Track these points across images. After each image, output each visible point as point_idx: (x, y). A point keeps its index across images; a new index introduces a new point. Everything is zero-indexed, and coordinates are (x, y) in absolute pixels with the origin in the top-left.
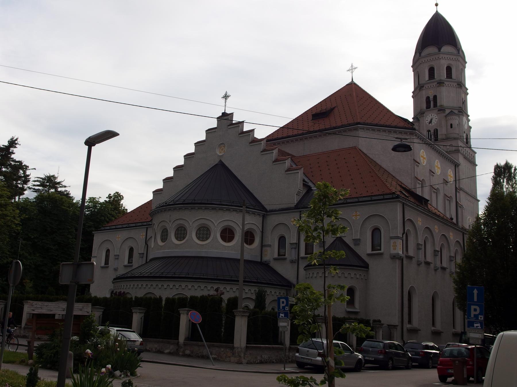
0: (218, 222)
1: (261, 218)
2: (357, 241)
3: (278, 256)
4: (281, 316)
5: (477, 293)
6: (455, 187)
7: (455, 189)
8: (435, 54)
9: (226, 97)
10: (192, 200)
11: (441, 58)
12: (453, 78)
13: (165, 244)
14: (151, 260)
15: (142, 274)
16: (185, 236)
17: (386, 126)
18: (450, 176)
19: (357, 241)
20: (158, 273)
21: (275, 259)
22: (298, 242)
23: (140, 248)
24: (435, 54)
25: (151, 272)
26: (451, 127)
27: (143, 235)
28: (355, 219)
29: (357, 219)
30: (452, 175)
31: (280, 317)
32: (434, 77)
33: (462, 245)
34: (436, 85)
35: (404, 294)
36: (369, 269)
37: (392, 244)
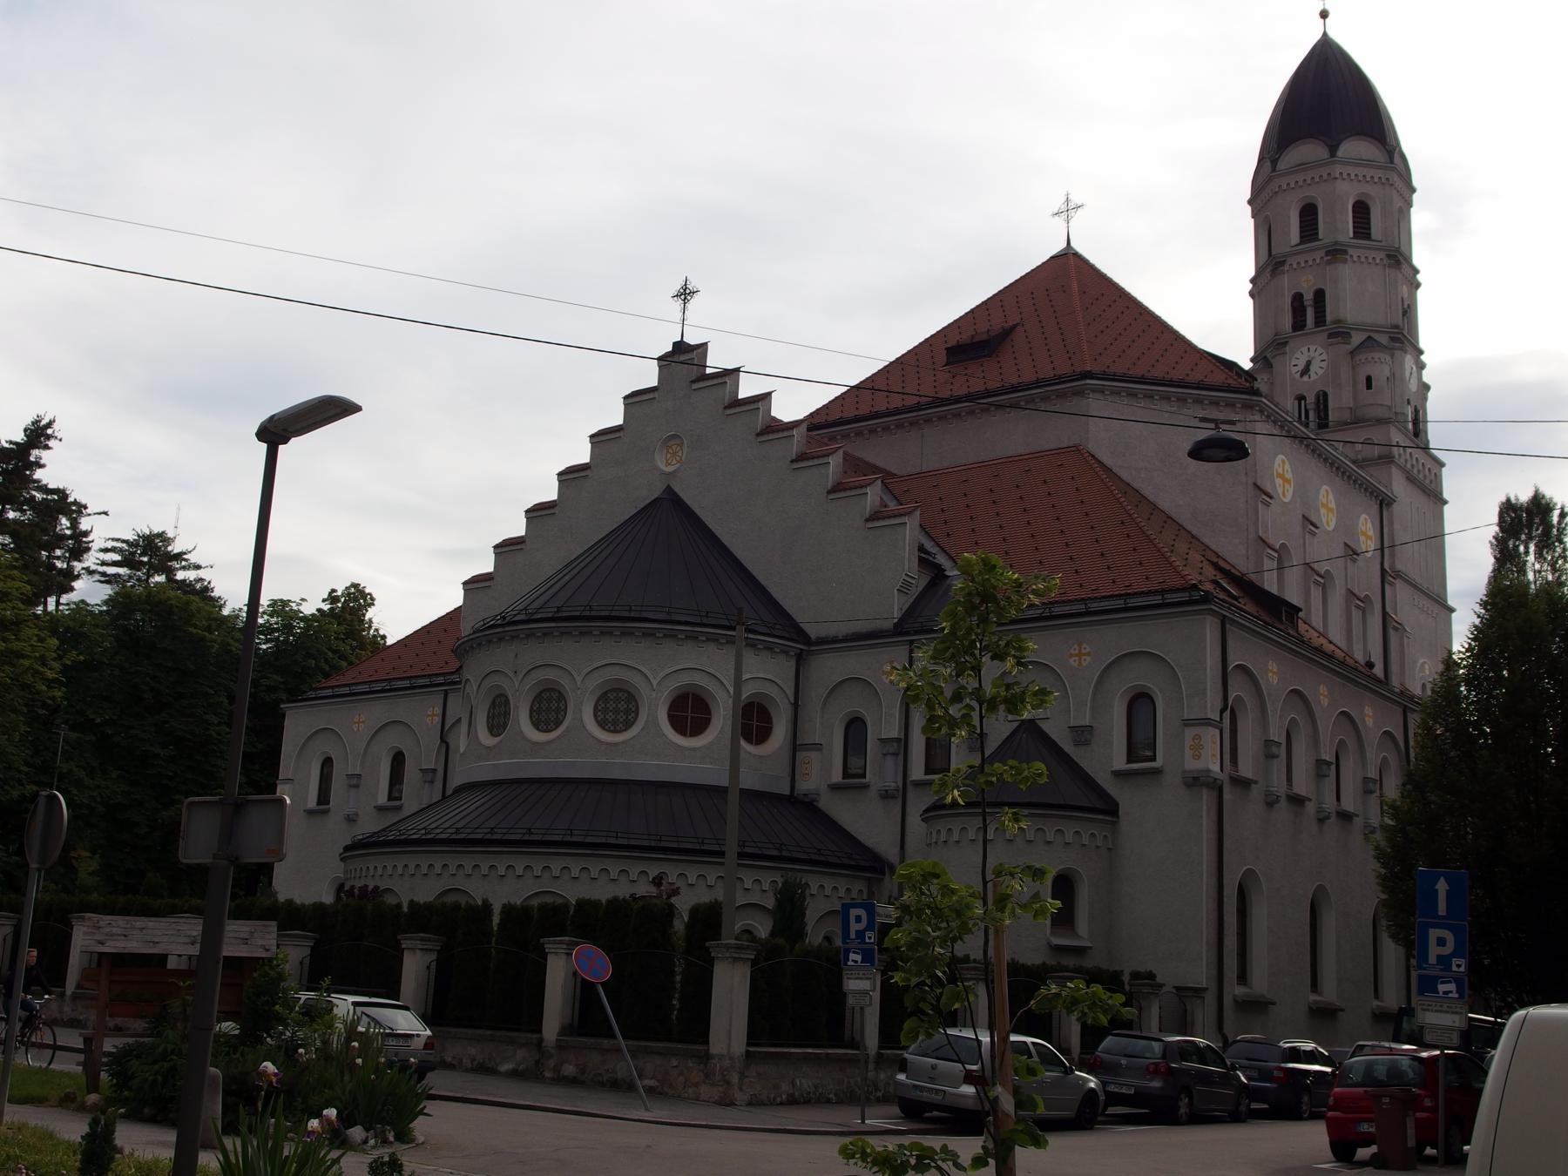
0: (662, 674)
1: (792, 663)
2: (1082, 731)
3: (843, 778)
4: (853, 961)
5: (1447, 891)
6: (1378, 567)
7: (1379, 573)
8: (1320, 164)
9: (685, 294)
10: (582, 608)
12: (1373, 237)
13: (501, 741)
14: (459, 790)
15: (429, 833)
16: (562, 718)
17: (1171, 384)
18: (1364, 534)
19: (1082, 731)
20: (478, 831)
21: (835, 788)
22: (902, 736)
23: (423, 755)
25: (459, 825)
26: (1369, 386)
27: (433, 715)
28: (1075, 664)
29: (1084, 664)
30: (1371, 533)
31: (849, 963)
32: (1317, 234)
33: (1402, 744)
34: (1322, 258)
35: (1226, 892)
36: (1118, 817)
37: (1188, 742)
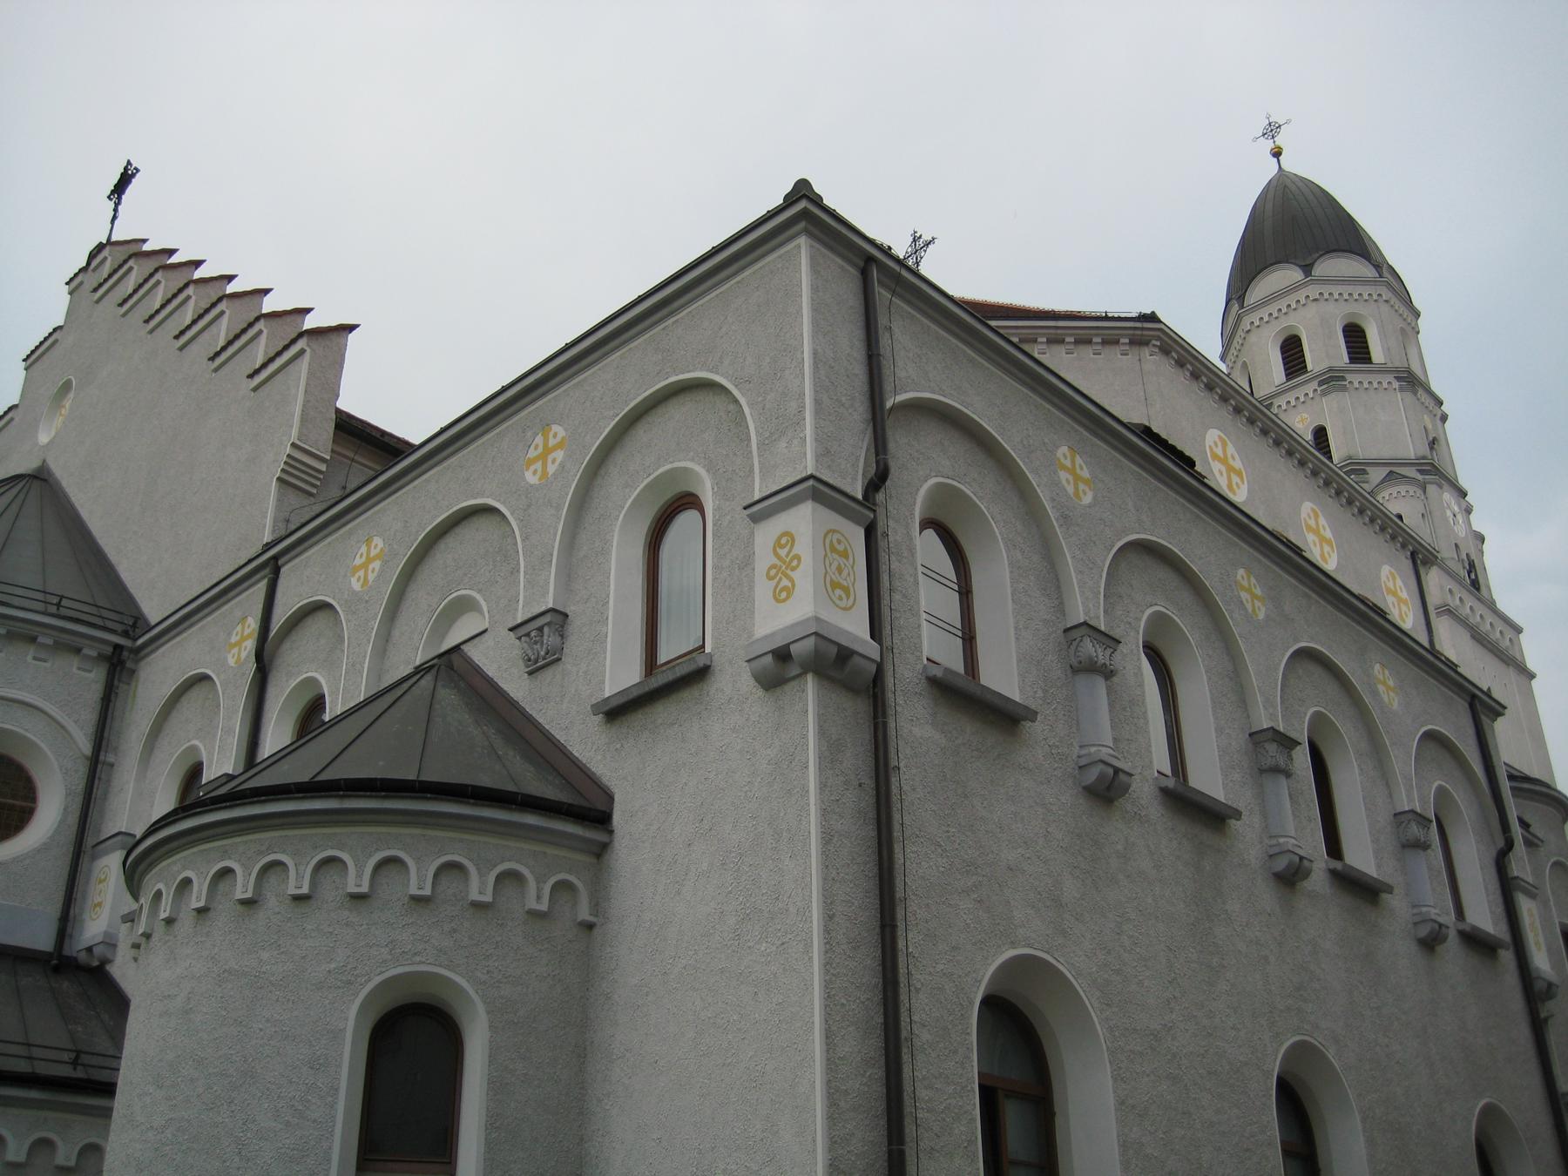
1: (95, 678)
2: (540, 629)
8: (1294, 288)
11: (1318, 297)
16: (489, 1092)
19: (540, 629)
24: (1294, 288)
30: (1404, 595)
36: (611, 832)
37: (764, 559)
